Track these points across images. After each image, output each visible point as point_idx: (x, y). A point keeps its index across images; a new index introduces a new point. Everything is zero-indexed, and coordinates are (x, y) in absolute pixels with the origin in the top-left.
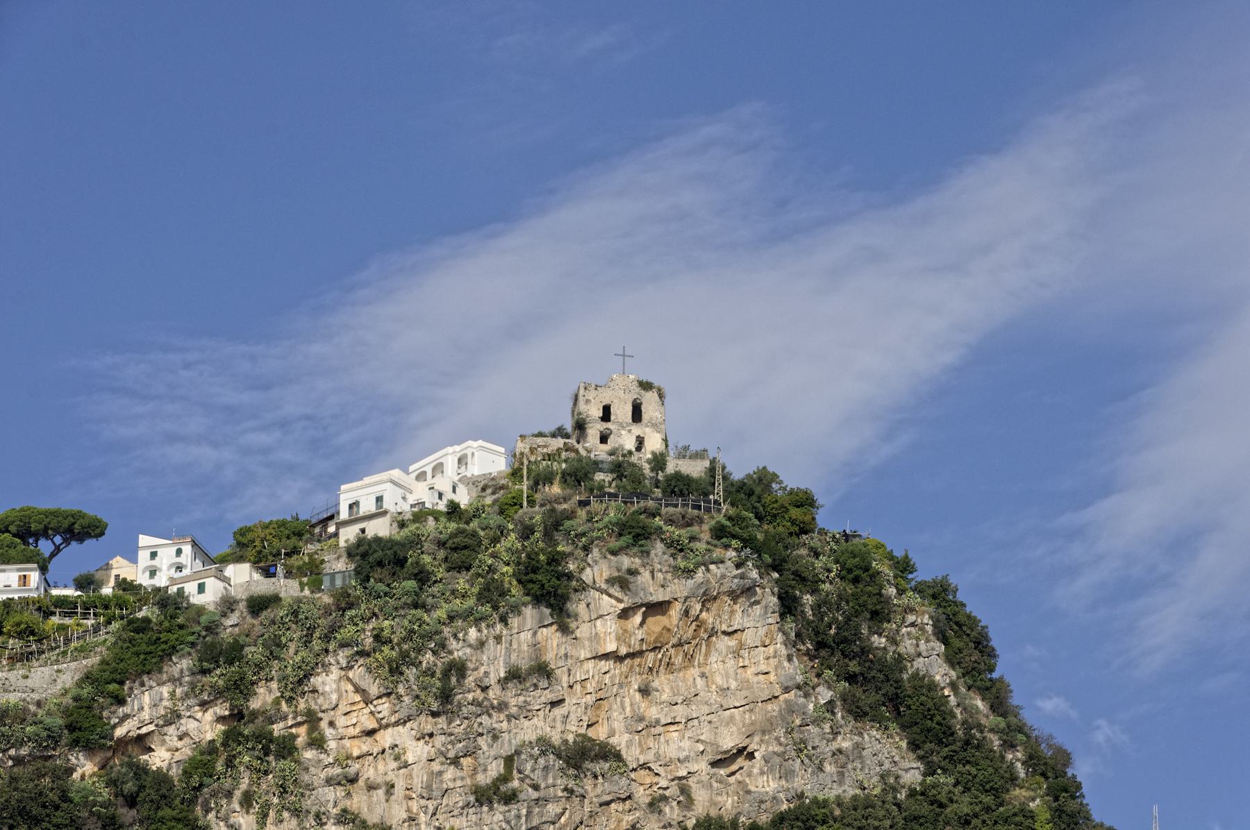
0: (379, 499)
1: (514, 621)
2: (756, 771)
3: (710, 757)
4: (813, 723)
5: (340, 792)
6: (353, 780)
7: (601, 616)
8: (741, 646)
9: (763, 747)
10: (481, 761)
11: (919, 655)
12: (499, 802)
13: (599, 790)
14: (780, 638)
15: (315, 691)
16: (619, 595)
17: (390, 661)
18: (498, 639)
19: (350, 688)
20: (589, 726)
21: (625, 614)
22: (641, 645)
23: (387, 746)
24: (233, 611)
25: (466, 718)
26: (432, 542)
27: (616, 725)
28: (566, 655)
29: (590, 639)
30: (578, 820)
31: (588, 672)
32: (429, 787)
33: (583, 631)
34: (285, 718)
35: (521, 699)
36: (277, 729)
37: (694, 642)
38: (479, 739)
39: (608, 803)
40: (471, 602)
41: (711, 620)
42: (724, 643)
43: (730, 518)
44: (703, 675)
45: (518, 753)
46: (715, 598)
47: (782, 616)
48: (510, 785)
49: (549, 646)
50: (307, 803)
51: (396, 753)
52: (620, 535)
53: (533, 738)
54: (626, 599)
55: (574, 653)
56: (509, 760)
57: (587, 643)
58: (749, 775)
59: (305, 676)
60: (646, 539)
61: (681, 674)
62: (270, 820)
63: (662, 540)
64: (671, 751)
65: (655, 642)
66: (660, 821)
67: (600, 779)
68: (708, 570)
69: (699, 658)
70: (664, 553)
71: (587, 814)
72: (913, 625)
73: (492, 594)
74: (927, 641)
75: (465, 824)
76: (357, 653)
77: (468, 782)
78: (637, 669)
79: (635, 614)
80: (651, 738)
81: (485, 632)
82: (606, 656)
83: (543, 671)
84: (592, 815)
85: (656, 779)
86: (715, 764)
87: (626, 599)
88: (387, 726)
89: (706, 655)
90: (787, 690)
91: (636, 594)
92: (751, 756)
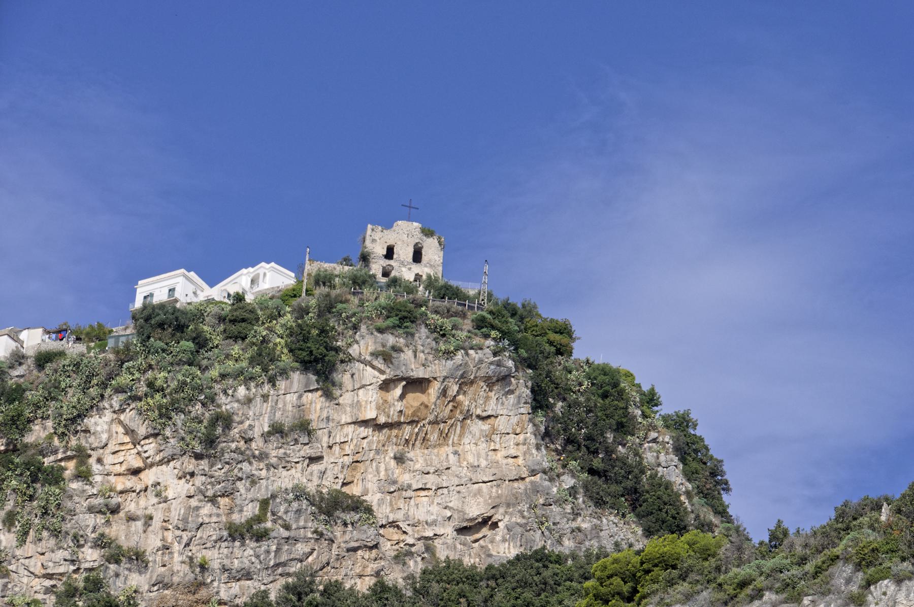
0: (172, 291)
1: (282, 384)
2: (498, 538)
3: (456, 523)
4: (555, 502)
5: (100, 519)
6: (115, 511)
7: (363, 386)
8: (494, 431)
9: (507, 518)
10: (238, 502)
11: (659, 465)
12: (251, 539)
13: (347, 537)
14: (530, 428)
15: (87, 431)
16: (382, 367)
17: (160, 407)
18: (265, 397)
19: (121, 430)
20: (344, 484)
21: (386, 386)
22: (399, 416)
23: (150, 483)
24: (20, 364)
25: (227, 463)
26: (214, 316)
27: (370, 485)
28: (328, 418)
29: (352, 406)
30: (324, 561)
31: (347, 435)
32: (185, 520)
33: (346, 399)
34: (55, 452)
35: (282, 451)
36: (48, 461)
37: (450, 422)
38: (238, 483)
39: (355, 550)
40: (244, 364)
41: (467, 403)
42: (478, 427)
43: (491, 312)
44: (456, 453)
45: (274, 497)
46: (472, 383)
47: (535, 409)
48: (263, 525)
49: (313, 409)
50: (67, 526)
51: (158, 489)
52: (388, 317)
53: (290, 486)
54: (388, 371)
55: (335, 416)
56: (264, 504)
57: (348, 409)
58: (492, 542)
59: (79, 416)
60: (412, 322)
61: (436, 451)
62: (30, 538)
63: (427, 325)
64: (420, 514)
65: (414, 414)
66: (404, 572)
67: (350, 527)
68: (467, 354)
69: (454, 438)
70: (428, 337)
71: (334, 557)
72: (654, 441)
73: (264, 357)
74: (667, 453)
75: (216, 556)
76: (130, 397)
77: (224, 519)
78: (395, 440)
79: (396, 387)
80: (402, 500)
81: (254, 390)
82: (365, 423)
83: (304, 427)
84: (339, 558)
85: (403, 537)
86: (461, 531)
87: (388, 371)
88: (152, 465)
89: (460, 436)
90: (533, 473)
91: (398, 368)
92: (495, 525)
